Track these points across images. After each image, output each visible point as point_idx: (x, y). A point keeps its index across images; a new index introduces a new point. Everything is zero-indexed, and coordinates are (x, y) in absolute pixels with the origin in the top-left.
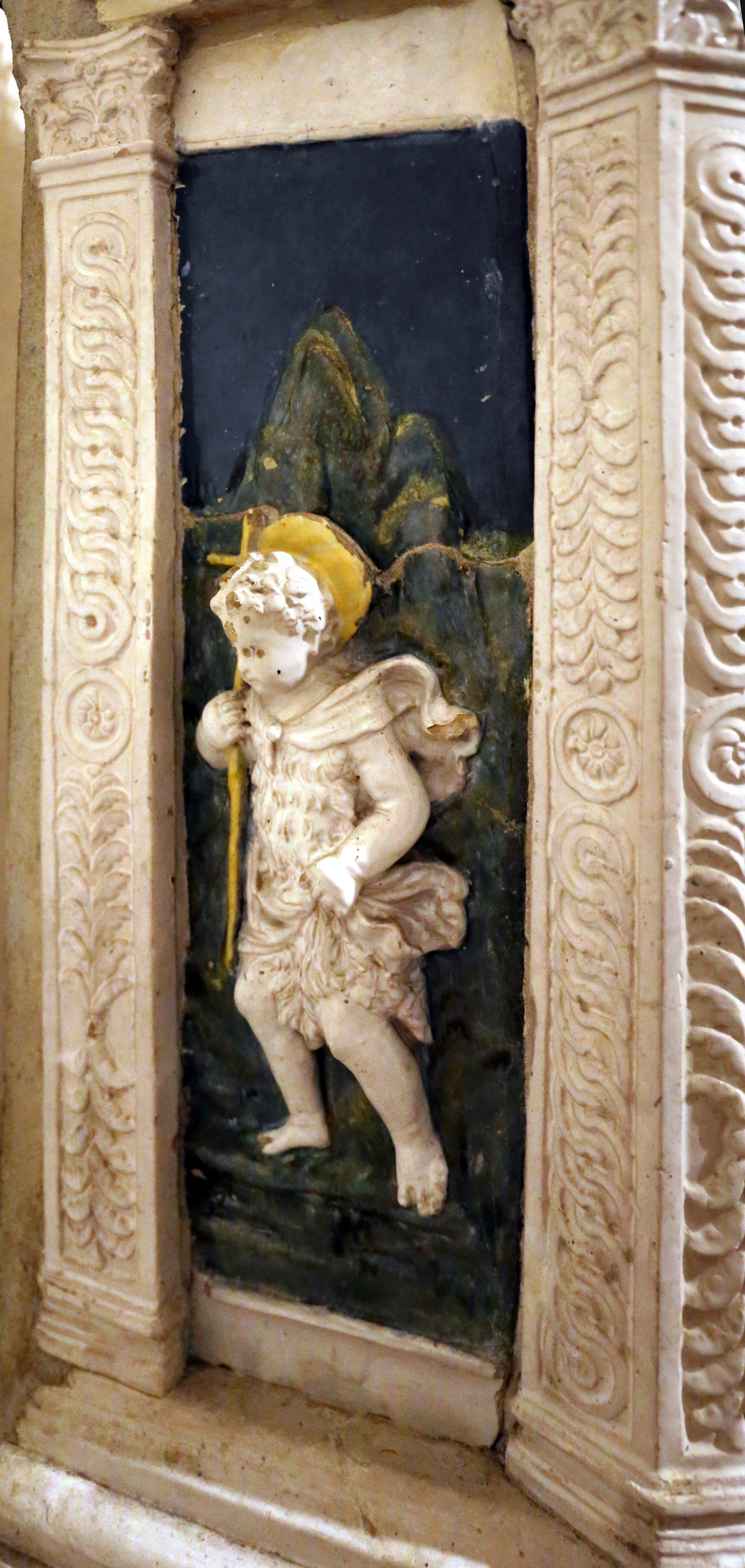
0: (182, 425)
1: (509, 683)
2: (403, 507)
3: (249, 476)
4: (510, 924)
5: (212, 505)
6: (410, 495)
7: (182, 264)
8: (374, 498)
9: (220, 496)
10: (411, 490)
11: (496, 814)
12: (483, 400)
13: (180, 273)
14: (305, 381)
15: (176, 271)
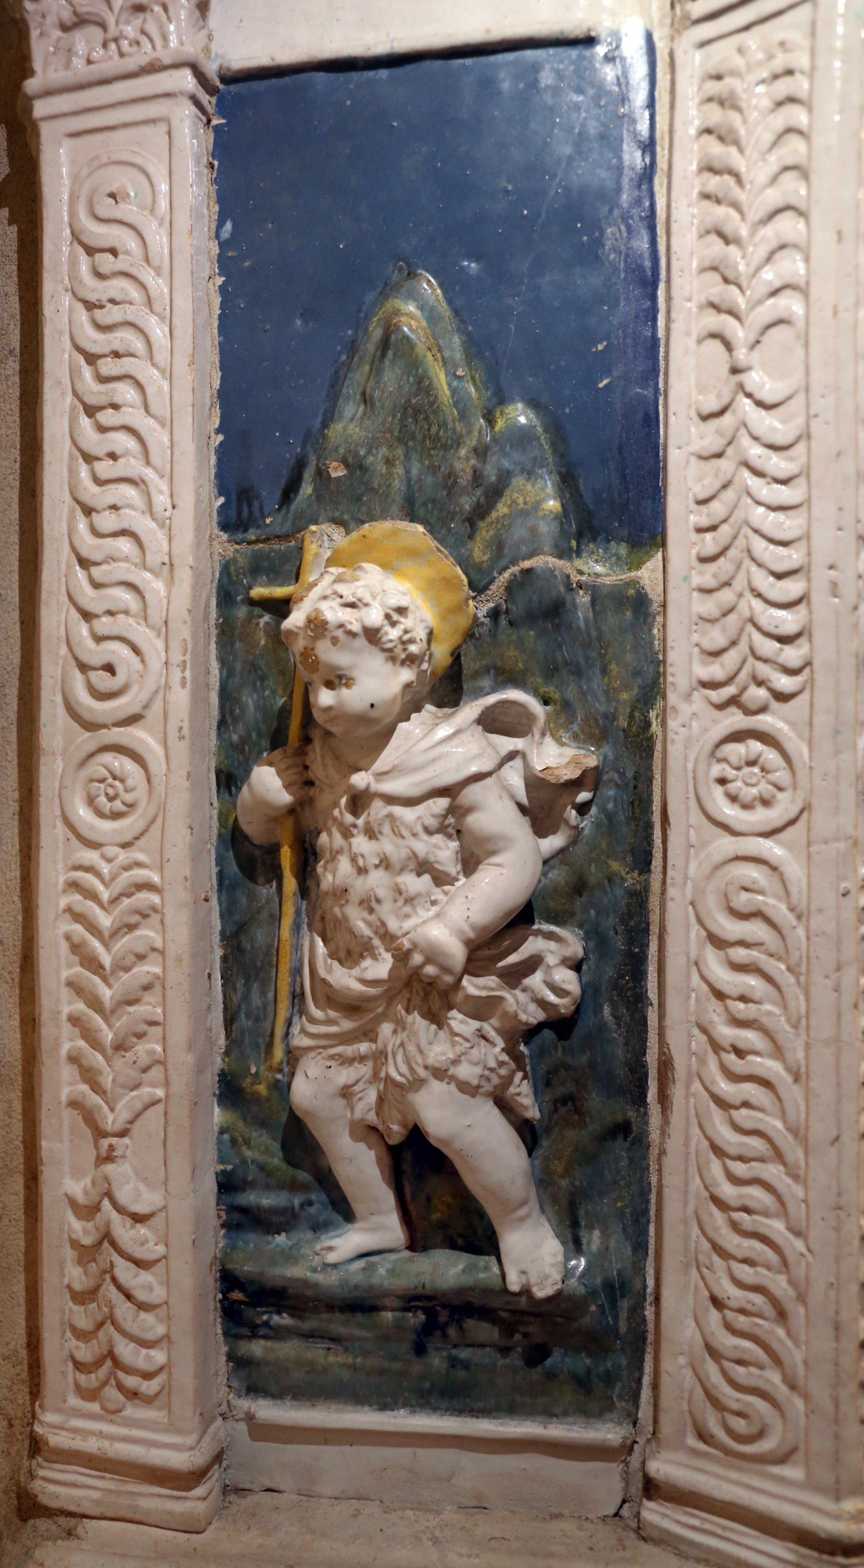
0: (218, 431)
1: (631, 716)
2: (505, 516)
3: (307, 489)
4: (631, 985)
5: (258, 527)
6: (514, 502)
7: (220, 224)
8: (467, 507)
9: (269, 515)
10: (515, 495)
11: (615, 866)
12: (601, 385)
13: (217, 236)
14: (387, 362)
15: (213, 234)
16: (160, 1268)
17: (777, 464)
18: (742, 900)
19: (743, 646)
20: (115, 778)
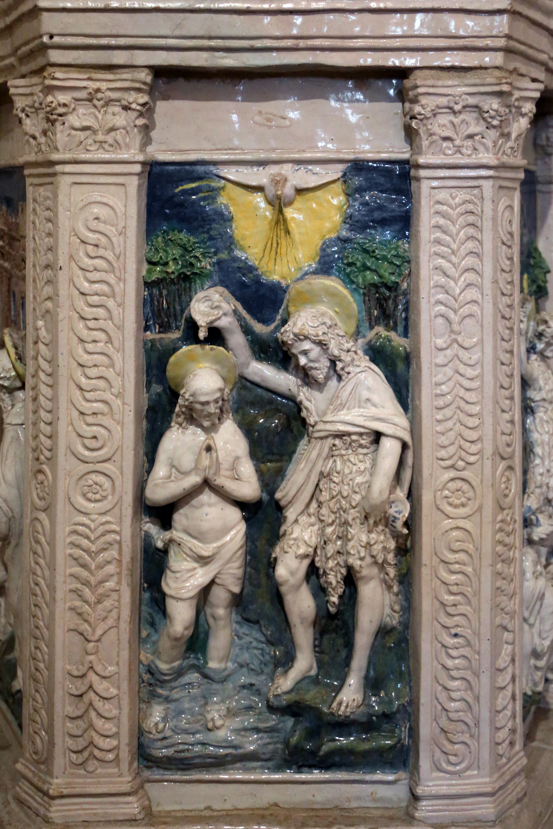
16: (115, 701)
17: (470, 372)
18: (457, 546)
19: (456, 446)
20: (96, 484)
